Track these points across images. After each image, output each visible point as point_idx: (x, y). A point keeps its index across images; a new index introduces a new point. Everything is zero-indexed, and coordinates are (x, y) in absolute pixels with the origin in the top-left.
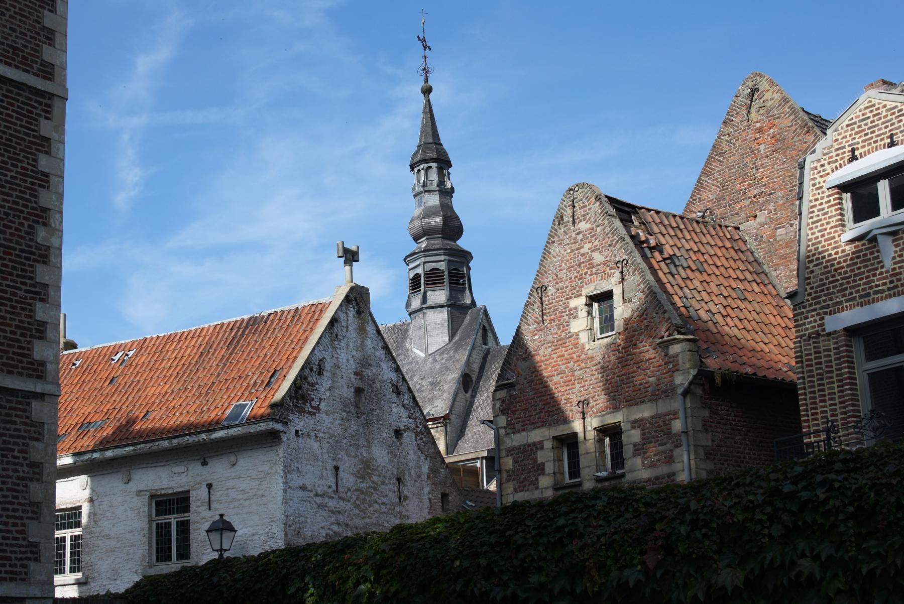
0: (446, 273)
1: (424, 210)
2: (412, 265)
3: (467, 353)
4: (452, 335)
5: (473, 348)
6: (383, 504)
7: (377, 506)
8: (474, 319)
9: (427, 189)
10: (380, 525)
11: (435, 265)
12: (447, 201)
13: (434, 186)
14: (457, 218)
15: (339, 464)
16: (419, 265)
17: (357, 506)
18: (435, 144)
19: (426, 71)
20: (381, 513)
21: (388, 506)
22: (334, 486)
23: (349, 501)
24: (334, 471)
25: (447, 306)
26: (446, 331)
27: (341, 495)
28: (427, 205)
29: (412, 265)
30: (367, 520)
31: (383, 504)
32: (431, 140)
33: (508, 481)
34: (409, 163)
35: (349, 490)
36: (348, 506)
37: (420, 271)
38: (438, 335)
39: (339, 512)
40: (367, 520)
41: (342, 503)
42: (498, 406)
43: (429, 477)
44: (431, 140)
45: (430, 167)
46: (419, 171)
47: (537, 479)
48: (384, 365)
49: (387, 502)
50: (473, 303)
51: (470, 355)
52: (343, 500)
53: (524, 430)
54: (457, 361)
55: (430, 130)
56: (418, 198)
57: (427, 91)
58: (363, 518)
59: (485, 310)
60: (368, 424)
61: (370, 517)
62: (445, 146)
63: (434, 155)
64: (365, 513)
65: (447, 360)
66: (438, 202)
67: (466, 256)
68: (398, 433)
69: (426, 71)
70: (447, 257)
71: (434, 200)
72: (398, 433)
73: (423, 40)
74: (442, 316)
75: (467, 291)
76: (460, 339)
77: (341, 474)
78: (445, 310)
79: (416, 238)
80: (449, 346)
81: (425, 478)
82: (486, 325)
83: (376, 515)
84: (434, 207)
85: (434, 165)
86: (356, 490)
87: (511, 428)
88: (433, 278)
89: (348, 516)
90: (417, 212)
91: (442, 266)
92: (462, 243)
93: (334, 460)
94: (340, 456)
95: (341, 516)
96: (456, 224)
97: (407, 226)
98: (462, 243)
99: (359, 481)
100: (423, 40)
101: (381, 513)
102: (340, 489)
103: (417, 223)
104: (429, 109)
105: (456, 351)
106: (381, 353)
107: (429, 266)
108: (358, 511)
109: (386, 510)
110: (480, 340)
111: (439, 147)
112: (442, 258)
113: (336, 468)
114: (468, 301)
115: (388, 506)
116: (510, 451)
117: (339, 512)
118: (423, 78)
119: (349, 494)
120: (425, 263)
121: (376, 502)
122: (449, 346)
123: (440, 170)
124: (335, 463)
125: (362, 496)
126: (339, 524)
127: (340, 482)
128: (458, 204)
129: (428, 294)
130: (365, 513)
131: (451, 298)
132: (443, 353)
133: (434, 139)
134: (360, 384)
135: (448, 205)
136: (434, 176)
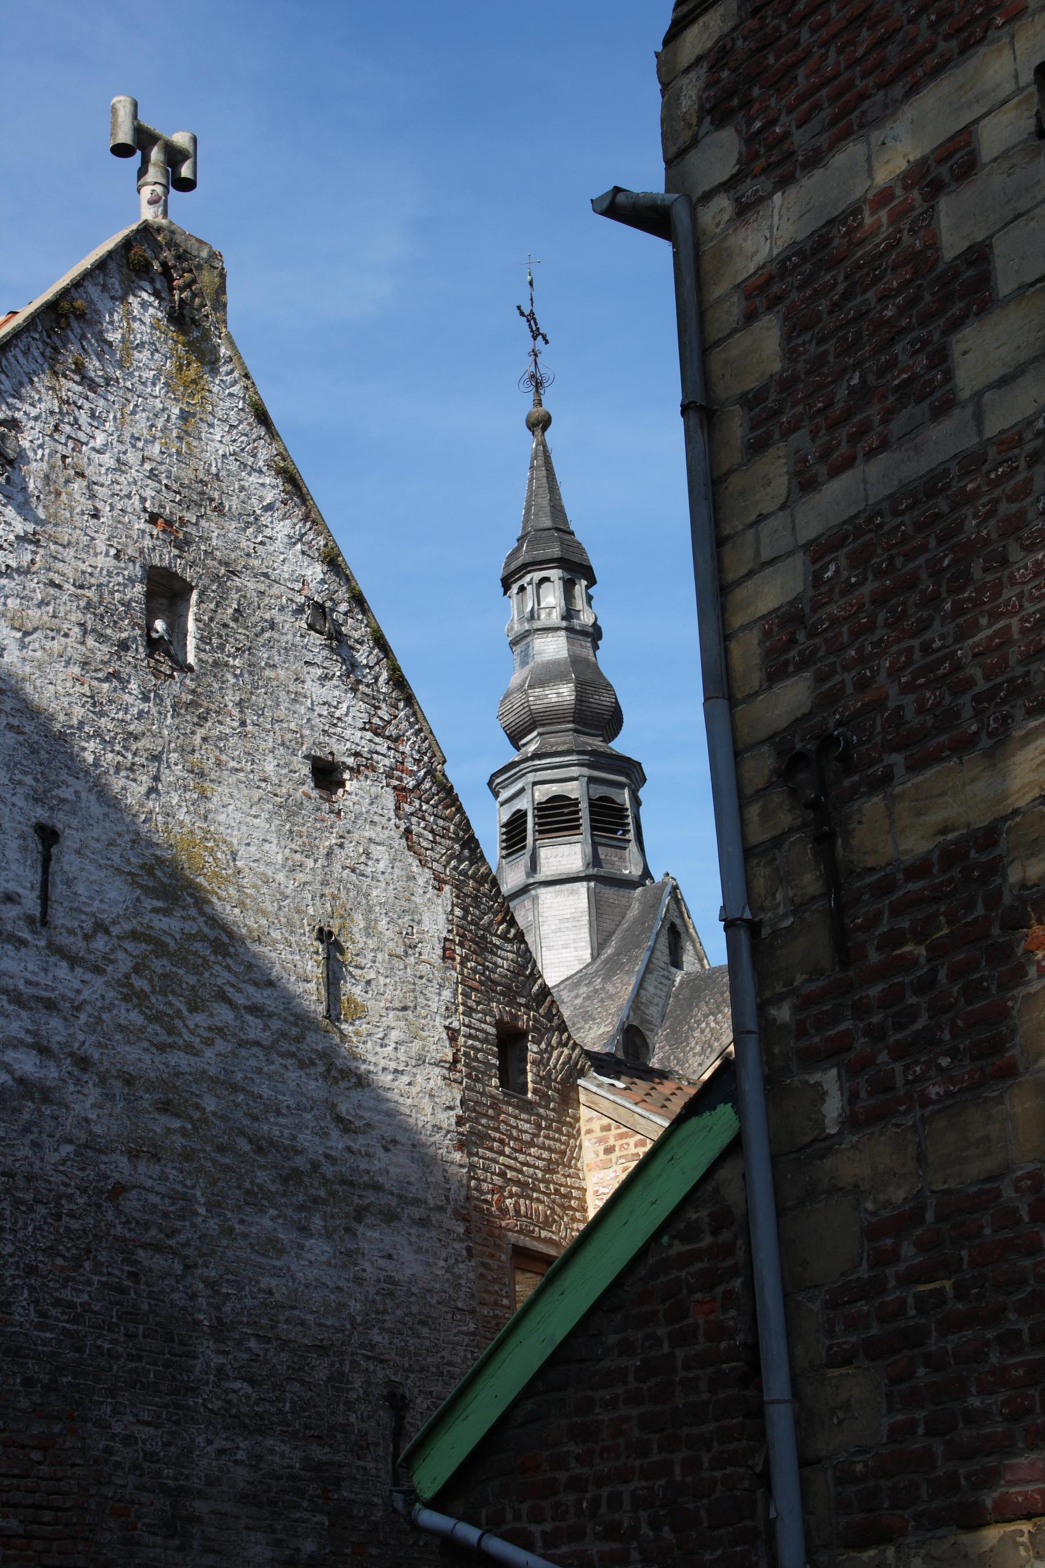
0: (584, 805)
1: (531, 671)
2: (505, 795)
3: (634, 980)
4: (598, 946)
5: (648, 970)
6: (255, 1010)
7: (225, 1015)
8: (651, 907)
9: (537, 625)
10: (235, 1088)
11: (555, 789)
12: (587, 652)
13: (555, 618)
14: (609, 687)
15: (59, 820)
16: (522, 790)
17: (133, 997)
18: (558, 529)
19: (537, 383)
20: (241, 1044)
21: (276, 1024)
22: (31, 902)
23: (98, 970)
24: (34, 843)
25: (587, 878)
26: (584, 934)
27: (64, 940)
28: (538, 659)
29: (505, 795)
30: (180, 1060)
31: (255, 1010)
32: (547, 523)
33: (756, 447)
34: (500, 573)
35: (101, 927)
36: (96, 989)
37: (524, 803)
38: (566, 946)
39: (50, 1006)
40: (180, 1060)
41: (62, 970)
42: (691, 89)
43: (447, 955)
44: (547, 523)
45: (545, 580)
46: (522, 589)
47: (941, 358)
48: (282, 529)
49: (271, 1006)
50: (646, 874)
51: (641, 985)
52: (74, 962)
53: (846, 134)
54: (611, 997)
55: (545, 502)
56: (517, 649)
57: (540, 424)
58: (162, 1048)
59: (675, 888)
60: (197, 709)
61: (190, 1049)
62: (578, 537)
63: (555, 551)
64: (171, 1031)
65: (588, 998)
66: (564, 654)
67: (632, 772)
68: (326, 775)
69: (537, 383)
70: (586, 771)
71: (553, 648)
72: (326, 775)
73: (531, 318)
74: (575, 901)
75: (633, 846)
76: (618, 953)
77: (67, 861)
78: (582, 888)
79: (515, 737)
80: (594, 967)
81: (432, 952)
82: (678, 922)
83: (221, 1045)
84: (556, 663)
85: (555, 574)
86: (134, 936)
87: (772, 164)
88: (556, 817)
89: (91, 1028)
90: (516, 678)
91: (574, 790)
92: (620, 745)
93: (37, 799)
94: (66, 793)
95: (56, 1022)
96: (606, 700)
97: (496, 710)
98: (620, 745)
99: (149, 903)
100: (531, 318)
101: (241, 1044)
102: (59, 916)
103: (517, 700)
104: (544, 459)
105: (608, 978)
106: (269, 488)
107: (542, 793)
108: (136, 1018)
109: (266, 1037)
110: (663, 955)
111: (566, 537)
112: (575, 771)
113: (48, 836)
114: (636, 871)
115: (276, 1024)
116: (763, 292)
117: (50, 1006)
118: (531, 396)
119: (100, 943)
120: (535, 784)
121: (223, 997)
122: (594, 967)
123: (568, 586)
124: (40, 813)
125: (160, 965)
126: (43, 1050)
127: (58, 891)
128: (608, 660)
129: (543, 853)
130: (171, 1031)
131: (595, 861)
132: (577, 985)
133: (554, 520)
134: (165, 557)
135: (587, 661)
136: (552, 597)
